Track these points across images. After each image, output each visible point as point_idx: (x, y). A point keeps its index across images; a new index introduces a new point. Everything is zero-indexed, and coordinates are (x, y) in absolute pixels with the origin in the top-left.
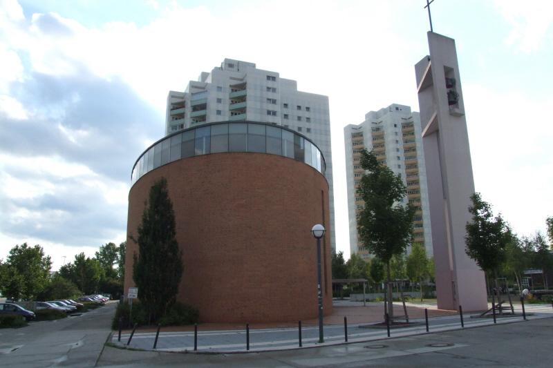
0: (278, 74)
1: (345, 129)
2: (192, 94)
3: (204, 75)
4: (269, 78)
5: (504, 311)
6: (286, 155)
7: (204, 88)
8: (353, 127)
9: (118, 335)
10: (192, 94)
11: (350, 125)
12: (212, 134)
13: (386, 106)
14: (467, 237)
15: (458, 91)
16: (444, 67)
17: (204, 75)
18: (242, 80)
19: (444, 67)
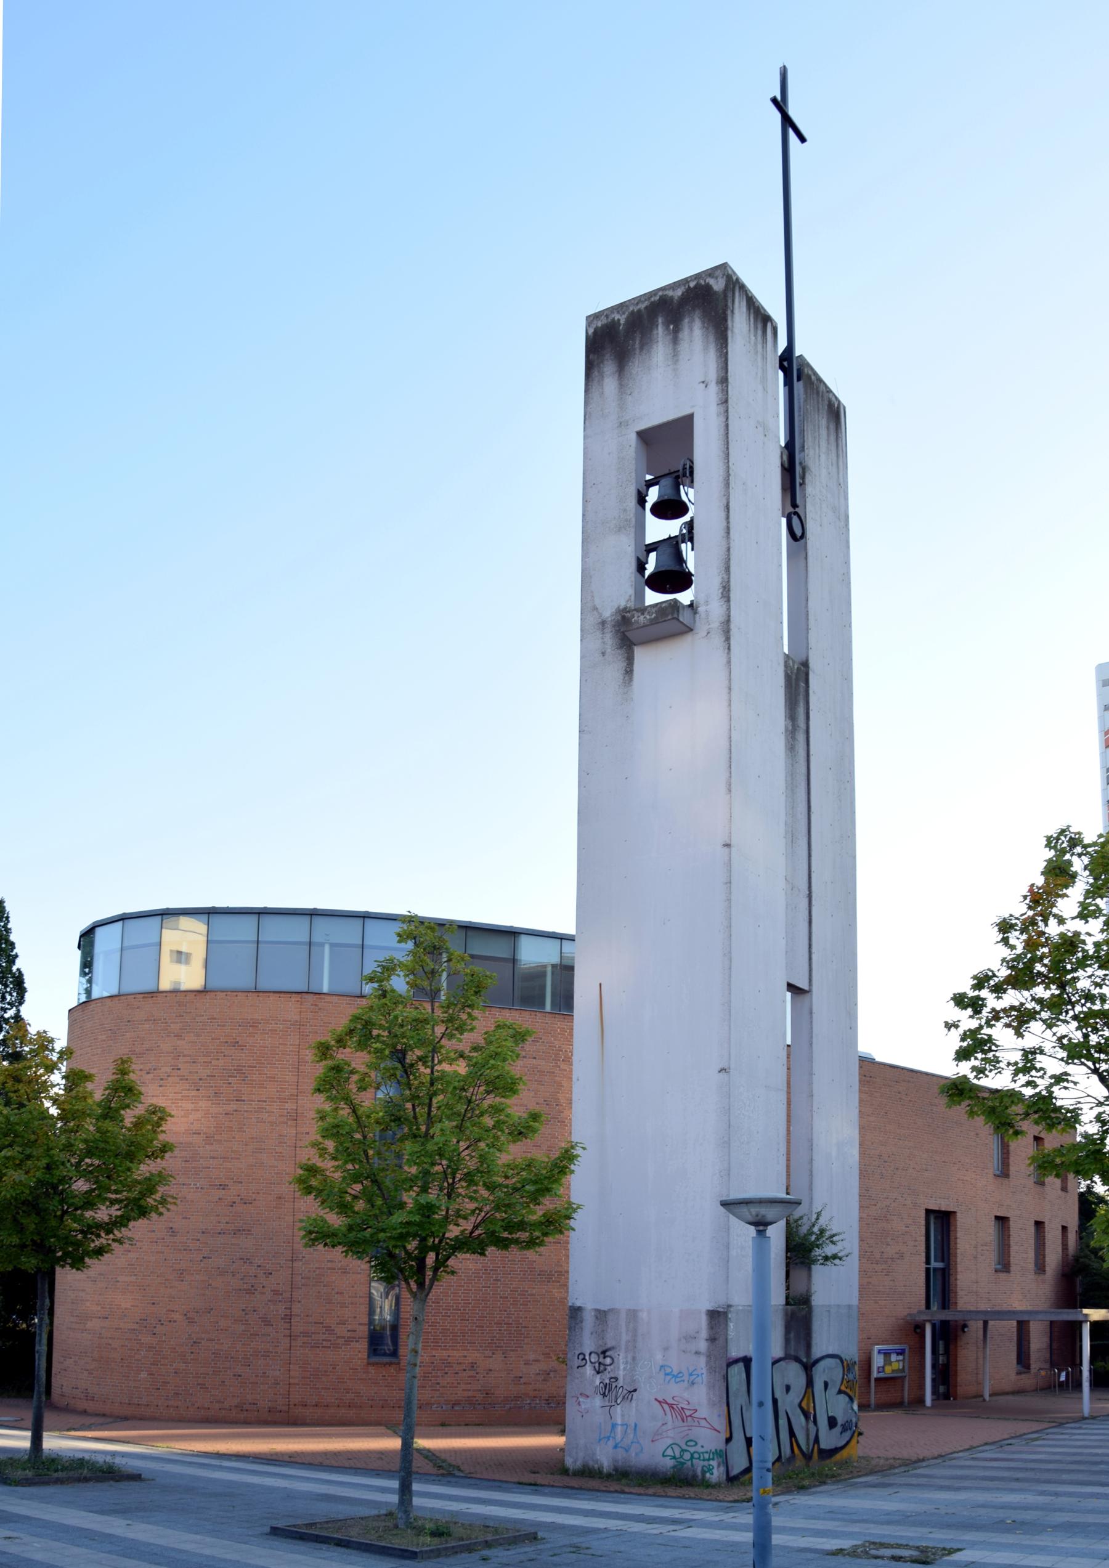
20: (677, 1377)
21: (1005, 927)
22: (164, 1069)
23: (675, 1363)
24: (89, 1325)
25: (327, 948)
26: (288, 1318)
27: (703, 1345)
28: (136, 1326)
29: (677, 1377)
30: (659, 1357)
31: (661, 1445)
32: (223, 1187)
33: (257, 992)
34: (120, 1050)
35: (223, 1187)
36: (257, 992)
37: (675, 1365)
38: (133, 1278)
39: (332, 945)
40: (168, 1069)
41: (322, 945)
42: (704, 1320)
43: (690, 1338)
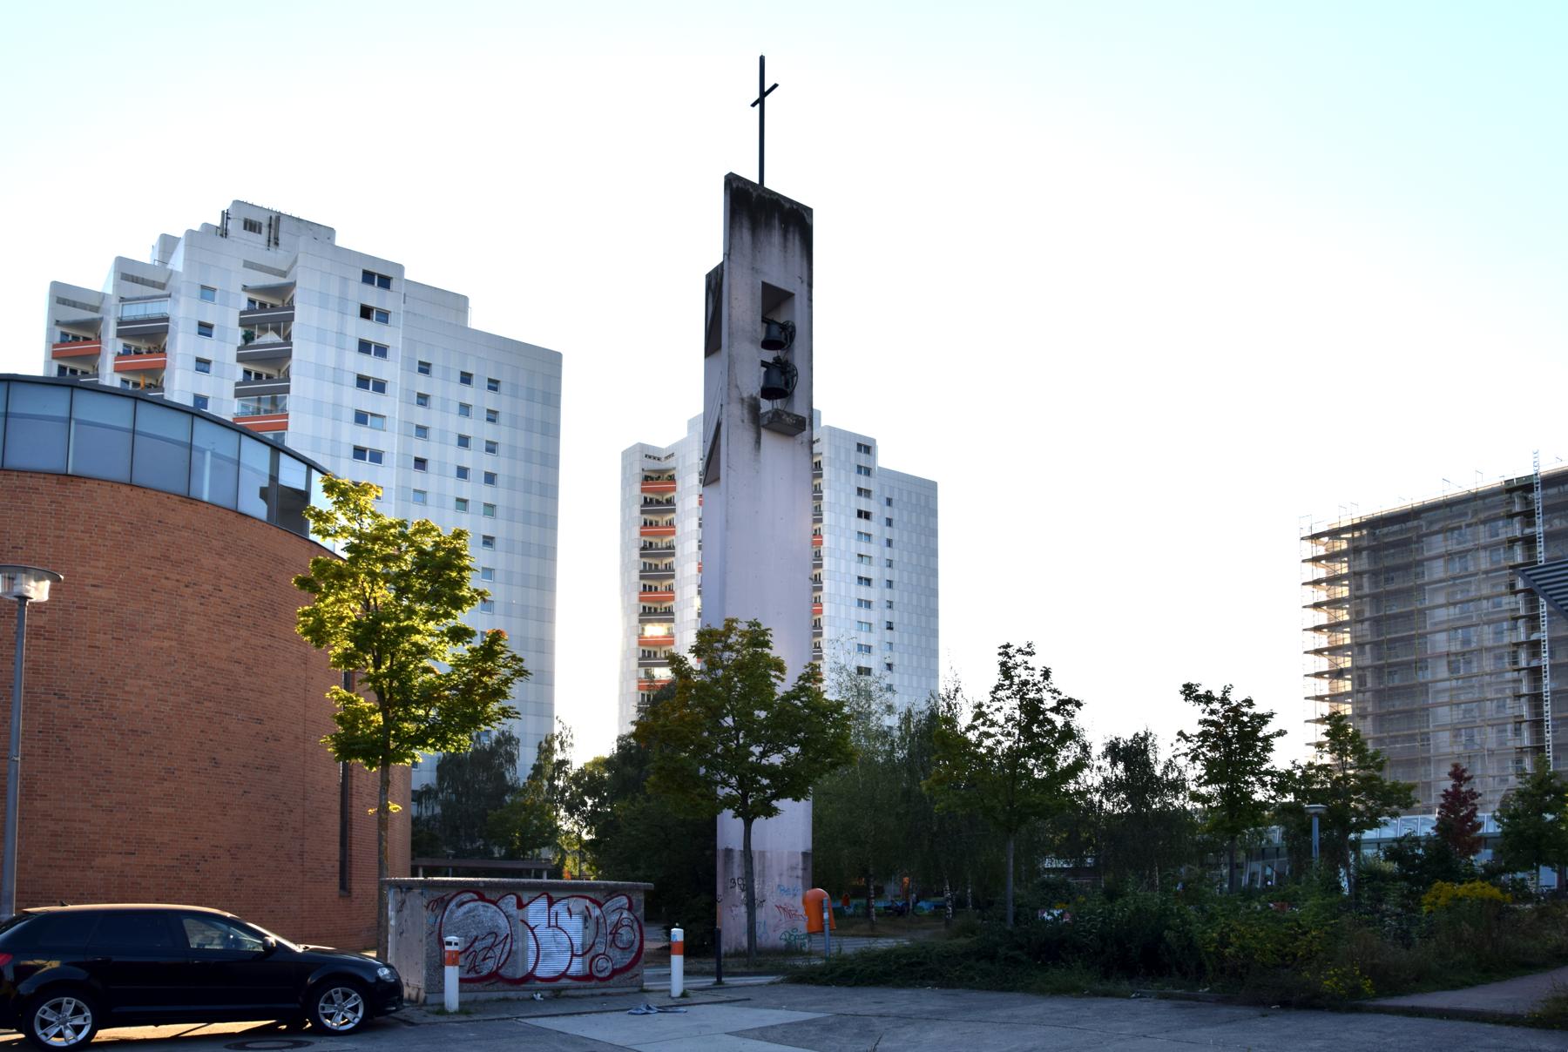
0: (400, 268)
1: (626, 455)
2: (122, 299)
3: (167, 244)
4: (368, 277)
5: (624, 901)
6: (206, 497)
7: (162, 286)
8: (649, 454)
9: (1488, 669)
10: (122, 299)
11: (642, 446)
12: (77, 415)
13: (1491, 477)
14: (915, 710)
15: (798, 362)
16: (765, 286)
17: (167, 244)
18: (283, 274)
19: (765, 286)
20: (786, 891)
21: (1250, 703)
22: (206, 587)
23: (785, 883)
24: (97, 862)
25: (208, 455)
26: (301, 854)
27: (800, 873)
28: (175, 863)
29: (786, 891)
30: (777, 880)
31: (779, 933)
32: (260, 721)
33: (131, 485)
34: (498, 607)
35: (260, 721)
36: (131, 485)
37: (785, 885)
38: (171, 810)
39: (214, 455)
40: (210, 588)
41: (203, 452)
42: (800, 857)
43: (793, 868)
